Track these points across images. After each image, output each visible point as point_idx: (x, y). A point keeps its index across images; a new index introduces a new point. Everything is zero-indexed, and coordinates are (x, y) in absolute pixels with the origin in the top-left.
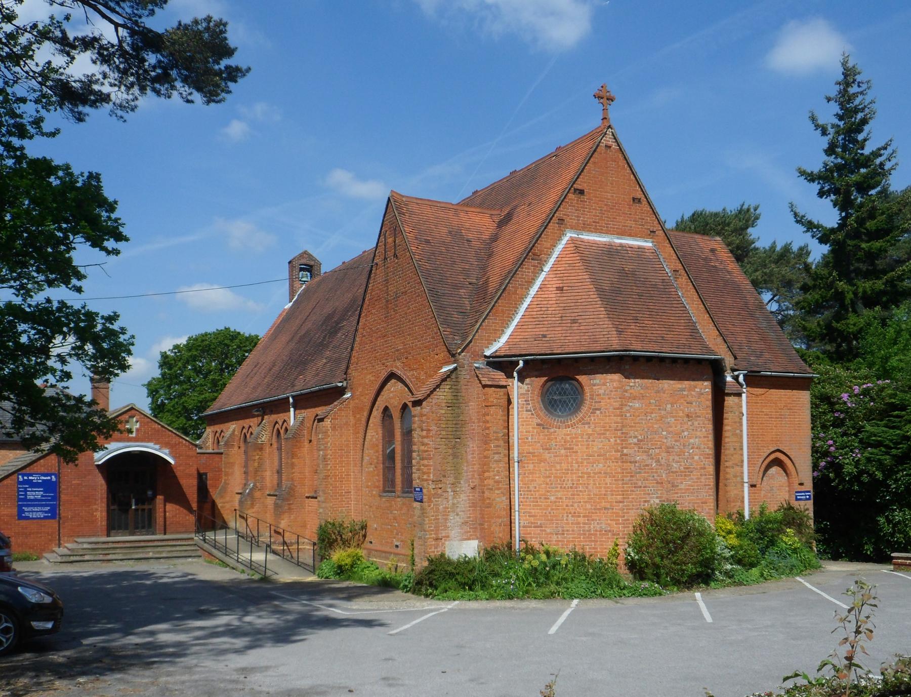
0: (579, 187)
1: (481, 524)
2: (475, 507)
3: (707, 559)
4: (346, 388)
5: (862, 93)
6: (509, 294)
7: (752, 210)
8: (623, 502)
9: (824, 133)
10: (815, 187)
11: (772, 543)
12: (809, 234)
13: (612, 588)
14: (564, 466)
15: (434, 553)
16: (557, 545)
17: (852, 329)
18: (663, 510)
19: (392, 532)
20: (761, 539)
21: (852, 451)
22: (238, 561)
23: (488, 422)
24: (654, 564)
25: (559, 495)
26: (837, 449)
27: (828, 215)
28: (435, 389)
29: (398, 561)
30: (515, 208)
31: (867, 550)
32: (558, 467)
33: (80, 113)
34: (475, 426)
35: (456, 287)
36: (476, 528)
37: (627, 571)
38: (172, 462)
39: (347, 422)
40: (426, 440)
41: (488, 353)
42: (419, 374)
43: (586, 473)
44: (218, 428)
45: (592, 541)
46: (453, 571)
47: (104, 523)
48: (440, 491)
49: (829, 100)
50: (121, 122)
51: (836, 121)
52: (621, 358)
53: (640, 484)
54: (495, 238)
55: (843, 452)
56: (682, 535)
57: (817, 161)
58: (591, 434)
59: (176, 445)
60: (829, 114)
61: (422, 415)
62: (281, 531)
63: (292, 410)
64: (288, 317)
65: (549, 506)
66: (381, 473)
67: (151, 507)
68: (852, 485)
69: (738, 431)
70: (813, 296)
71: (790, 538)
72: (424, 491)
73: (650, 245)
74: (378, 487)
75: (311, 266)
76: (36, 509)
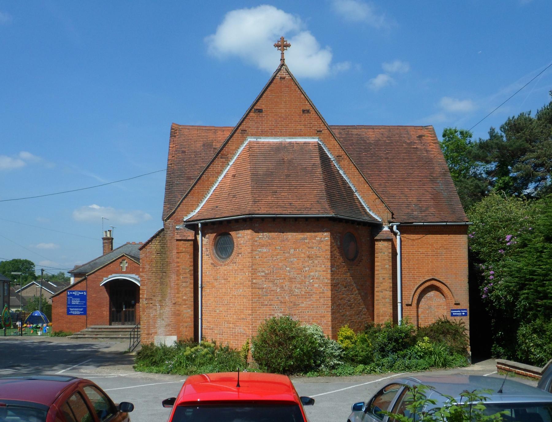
0: (258, 108)
6: (203, 181)
25: (221, 309)
31: (518, 355)
47: (108, 318)
48: (151, 305)
53: (266, 303)
67: (133, 309)
76: (76, 309)
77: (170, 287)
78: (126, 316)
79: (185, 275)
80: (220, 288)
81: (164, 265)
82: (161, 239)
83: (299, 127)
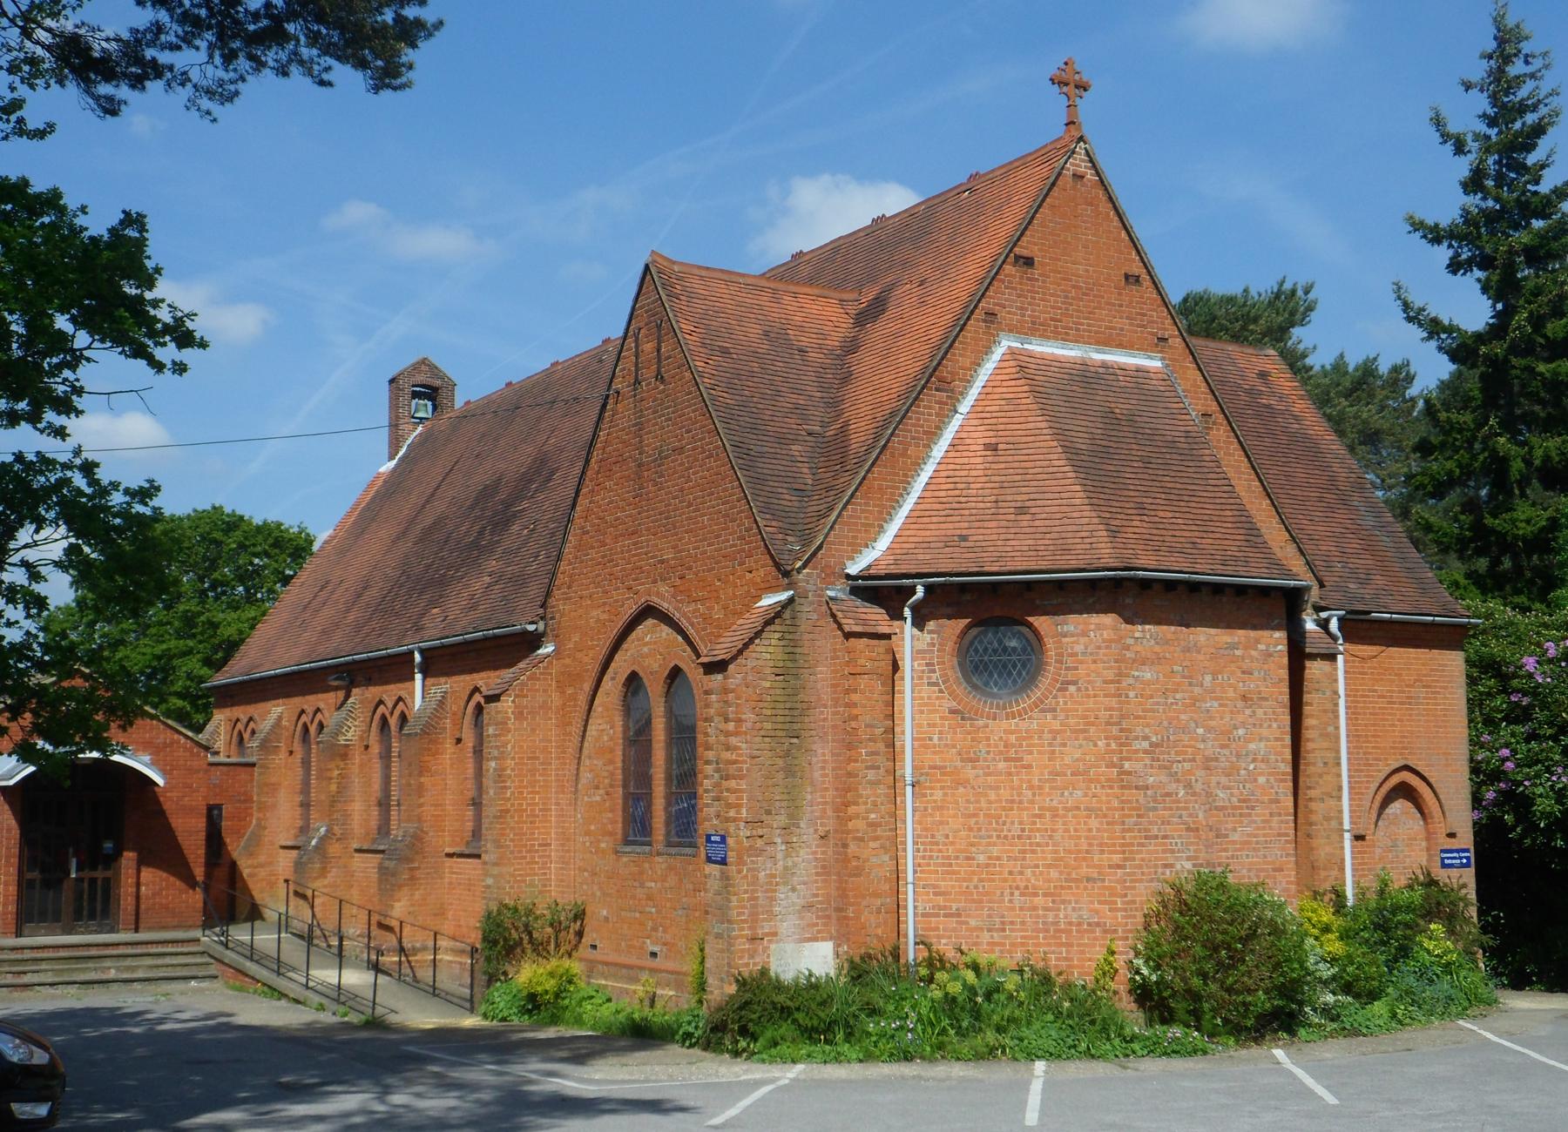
0: (1025, 253)
1: (838, 910)
2: (828, 874)
3: (1293, 981)
4: (543, 634)
5: (1533, 76)
7: (1300, 293)
8: (1123, 867)
9: (1460, 149)
10: (1443, 253)
11: (1404, 952)
12: (1433, 344)
13: (1108, 1039)
14: (1005, 793)
15: (748, 966)
16: (992, 951)
17: (1524, 530)
18: (1201, 882)
19: (641, 924)
20: (1384, 943)
21: (1548, 770)
22: (307, 987)
23: (854, 705)
24: (1189, 991)
25: (995, 851)
26: (1518, 765)
27: (1470, 308)
28: (751, 640)
29: (658, 984)
30: (890, 288)
33: (110, 99)
34: (828, 712)
35: (783, 440)
36: (828, 917)
37: (1134, 1006)
38: (160, 781)
39: (545, 702)
40: (733, 740)
41: (853, 570)
42: (710, 608)
43: (1049, 809)
44: (241, 712)
45: (1061, 945)
46: (789, 1003)
48: (759, 843)
49: (1468, 86)
50: (207, 121)
51: (1482, 128)
52: (1117, 583)
53: (1155, 830)
54: (852, 346)
56: (1243, 933)
57: (1449, 206)
58: (1058, 732)
59: (165, 745)
60: (1469, 112)
61: (726, 691)
62: (395, 924)
63: (418, 677)
64: (390, 489)
65: (973, 873)
66: (620, 807)
67: (109, 874)
68: (1551, 839)
69: (1331, 729)
70: (1440, 466)
71: (1436, 942)
72: (730, 841)
73: (1158, 364)
74: (611, 834)
75: (435, 390)
77: (812, 784)
78: (79, 897)
79: (872, 747)
80: (991, 788)
81: (796, 713)
82: (784, 628)
83: (1120, 322)
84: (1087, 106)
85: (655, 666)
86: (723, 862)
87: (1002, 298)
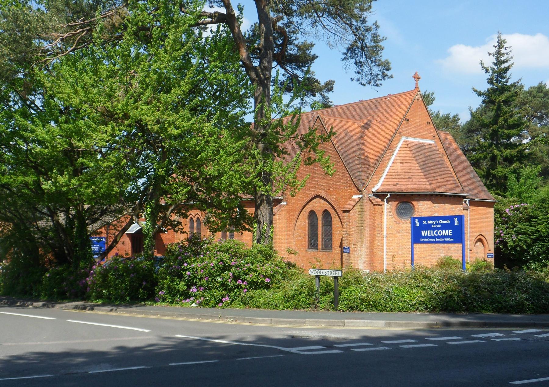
5: (507, 54)
9: (487, 71)
17: (500, 174)
25: (403, 252)
32: (403, 240)
34: (368, 221)
35: (353, 159)
41: (374, 190)
49: (490, 54)
51: (494, 66)
54: (362, 135)
55: (507, 236)
60: (490, 61)
83: (426, 133)
84: (419, 82)
85: (319, 209)
86: (349, 253)
87: (403, 129)
